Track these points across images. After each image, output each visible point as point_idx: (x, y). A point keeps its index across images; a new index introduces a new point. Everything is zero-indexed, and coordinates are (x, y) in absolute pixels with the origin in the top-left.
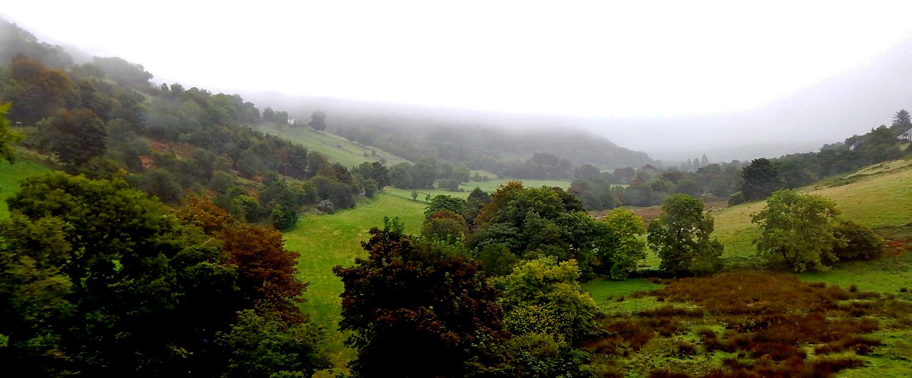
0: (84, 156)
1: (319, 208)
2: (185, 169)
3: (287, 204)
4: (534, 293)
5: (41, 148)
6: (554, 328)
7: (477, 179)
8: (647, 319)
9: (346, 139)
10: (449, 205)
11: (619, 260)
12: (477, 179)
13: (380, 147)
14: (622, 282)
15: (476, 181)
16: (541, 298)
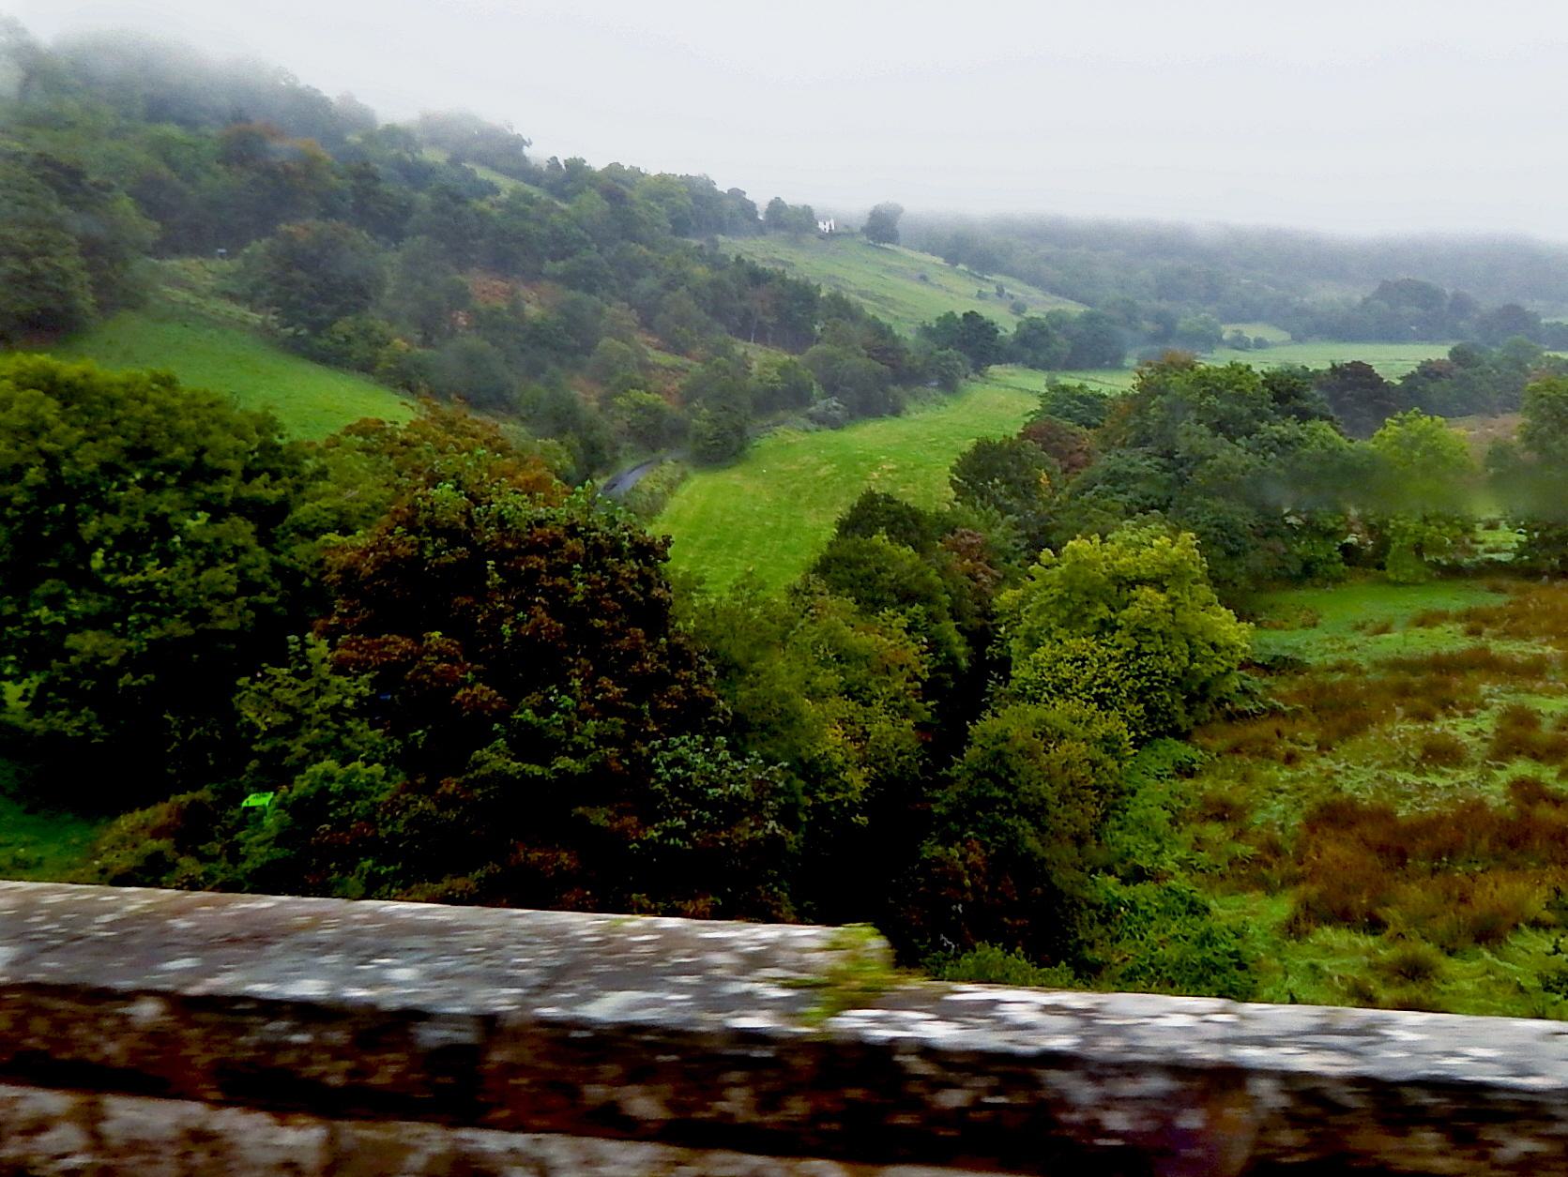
0: (325, 316)
1: (811, 417)
2: (538, 337)
3: (725, 409)
4: (1087, 610)
5: (249, 299)
6: (1119, 691)
7: (1240, 344)
8: (1403, 676)
9: (940, 261)
10: (1076, 407)
11: (1404, 535)
12: (1240, 344)
13: (1020, 277)
14: (1415, 588)
15: (1237, 349)
16: (1103, 622)
